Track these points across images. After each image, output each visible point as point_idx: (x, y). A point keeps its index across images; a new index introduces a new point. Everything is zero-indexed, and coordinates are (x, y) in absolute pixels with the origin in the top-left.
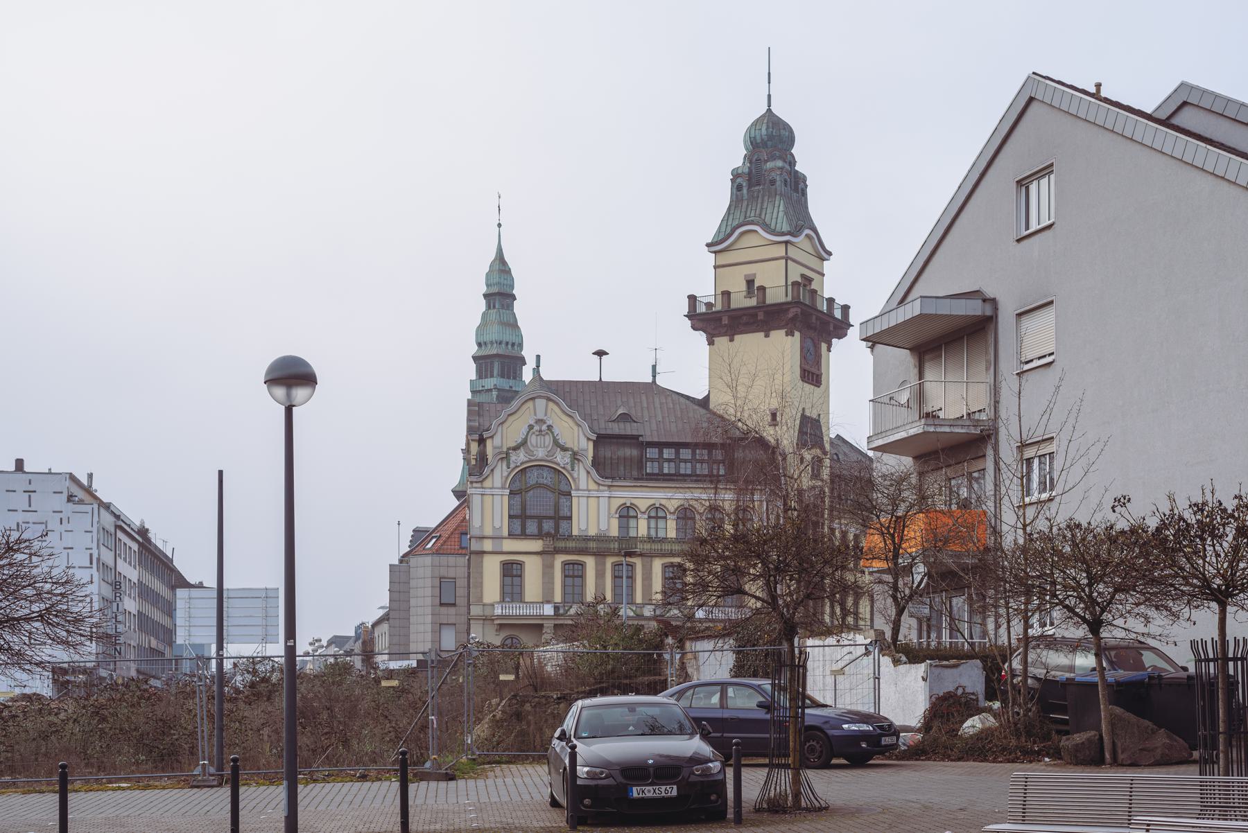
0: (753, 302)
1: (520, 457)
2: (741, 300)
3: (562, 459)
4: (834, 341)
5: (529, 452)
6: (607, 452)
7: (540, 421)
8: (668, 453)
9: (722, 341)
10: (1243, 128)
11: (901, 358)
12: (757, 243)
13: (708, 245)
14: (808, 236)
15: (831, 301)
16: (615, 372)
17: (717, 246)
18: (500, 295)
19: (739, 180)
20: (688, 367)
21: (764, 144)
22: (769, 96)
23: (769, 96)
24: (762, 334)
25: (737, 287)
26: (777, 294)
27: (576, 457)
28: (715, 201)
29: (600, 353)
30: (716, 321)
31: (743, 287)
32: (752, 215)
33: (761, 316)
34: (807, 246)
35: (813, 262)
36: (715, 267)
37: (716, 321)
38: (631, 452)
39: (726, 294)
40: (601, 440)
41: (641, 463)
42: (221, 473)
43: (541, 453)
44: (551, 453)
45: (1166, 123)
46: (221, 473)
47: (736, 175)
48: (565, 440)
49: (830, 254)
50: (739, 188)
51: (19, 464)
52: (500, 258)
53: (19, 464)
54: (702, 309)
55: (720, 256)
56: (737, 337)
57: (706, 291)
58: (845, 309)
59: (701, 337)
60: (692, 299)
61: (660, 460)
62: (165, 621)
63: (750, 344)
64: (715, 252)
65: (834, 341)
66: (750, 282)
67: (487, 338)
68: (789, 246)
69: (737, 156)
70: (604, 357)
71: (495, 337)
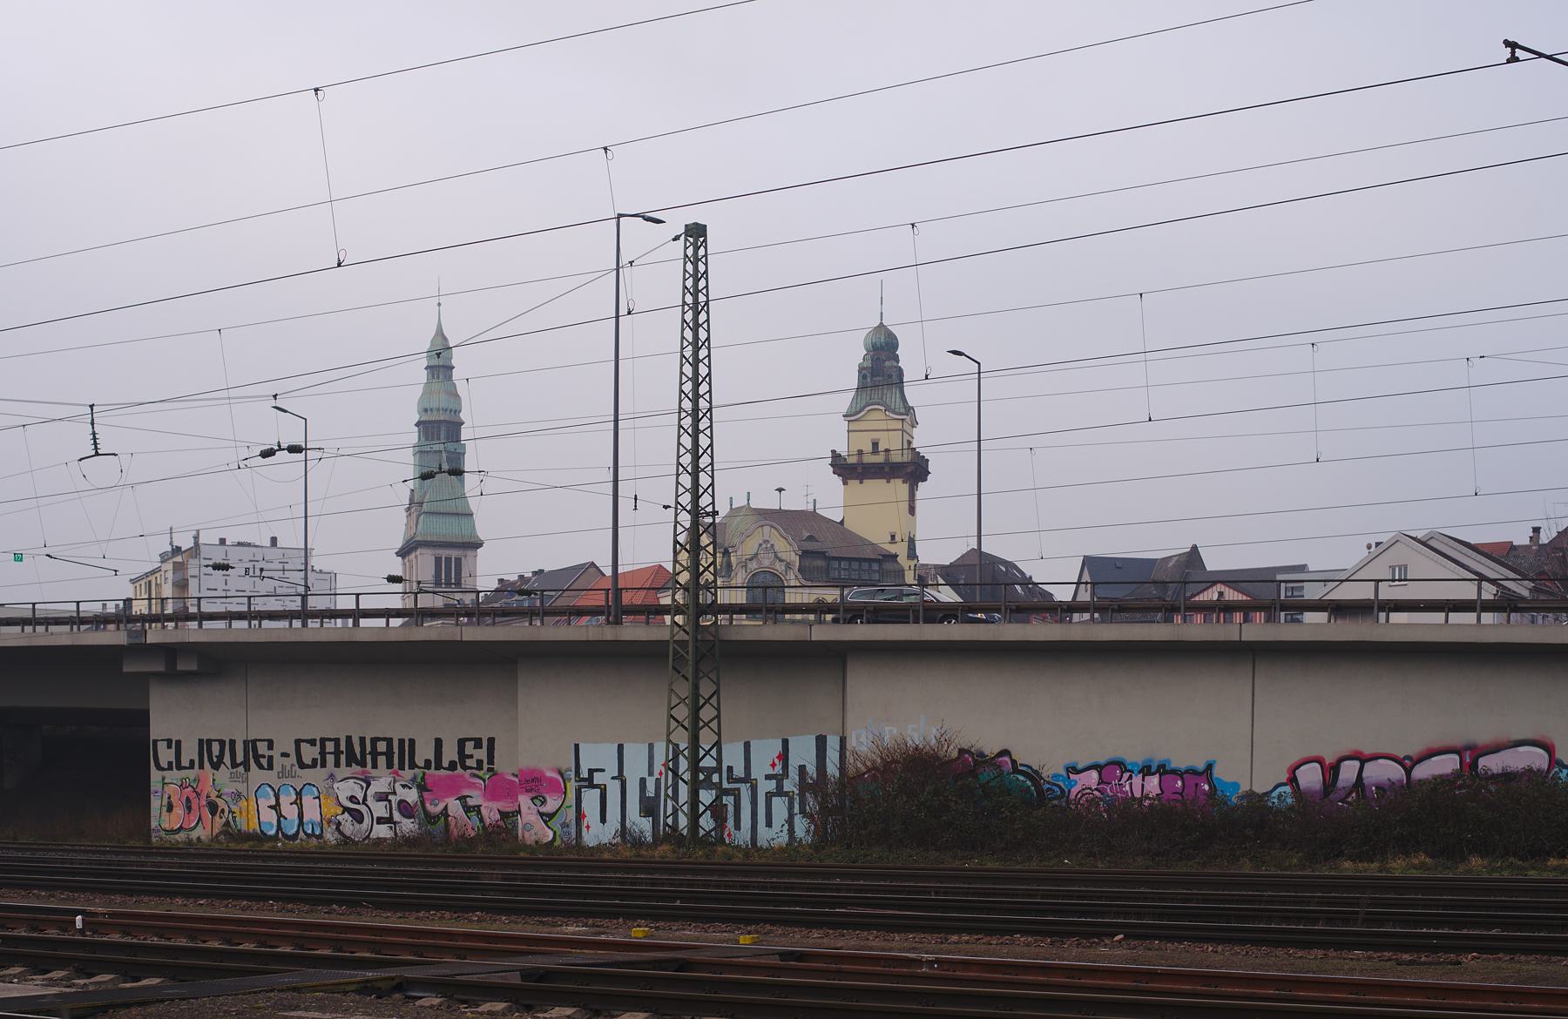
1: (753, 565)
3: (780, 567)
5: (759, 562)
6: (807, 563)
7: (766, 541)
8: (855, 565)
9: (854, 483)
12: (877, 419)
16: (788, 505)
18: (440, 365)
20: (830, 498)
21: (882, 348)
27: (788, 566)
29: (780, 490)
30: (846, 469)
37: (846, 469)
38: (820, 563)
39: (860, 452)
40: (805, 554)
41: (827, 571)
43: (766, 563)
44: (773, 563)
45: (1424, 544)
47: (861, 369)
48: (783, 556)
50: (864, 377)
51: (274, 541)
52: (440, 333)
53: (274, 541)
59: (838, 480)
61: (839, 569)
63: (876, 488)
66: (875, 445)
67: (435, 405)
71: (443, 405)
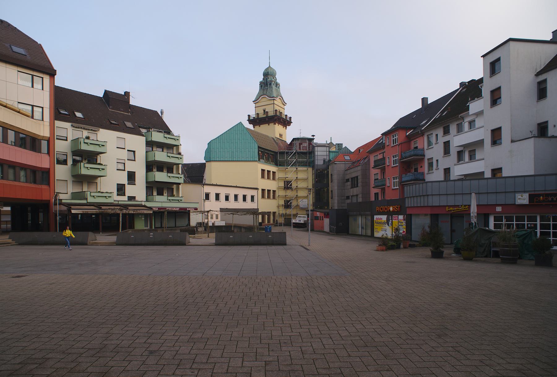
0: (265, 116)
2: (261, 116)
10: (5, 101)
11: (47, 139)
12: (264, 101)
15: (286, 116)
25: (261, 112)
26: (271, 114)
28: (256, 89)
31: (263, 112)
32: (265, 92)
33: (267, 119)
34: (279, 101)
35: (282, 106)
39: (258, 114)
54: (251, 118)
58: (290, 118)
60: (249, 116)
62: (74, 157)
66: (264, 111)
69: (261, 78)
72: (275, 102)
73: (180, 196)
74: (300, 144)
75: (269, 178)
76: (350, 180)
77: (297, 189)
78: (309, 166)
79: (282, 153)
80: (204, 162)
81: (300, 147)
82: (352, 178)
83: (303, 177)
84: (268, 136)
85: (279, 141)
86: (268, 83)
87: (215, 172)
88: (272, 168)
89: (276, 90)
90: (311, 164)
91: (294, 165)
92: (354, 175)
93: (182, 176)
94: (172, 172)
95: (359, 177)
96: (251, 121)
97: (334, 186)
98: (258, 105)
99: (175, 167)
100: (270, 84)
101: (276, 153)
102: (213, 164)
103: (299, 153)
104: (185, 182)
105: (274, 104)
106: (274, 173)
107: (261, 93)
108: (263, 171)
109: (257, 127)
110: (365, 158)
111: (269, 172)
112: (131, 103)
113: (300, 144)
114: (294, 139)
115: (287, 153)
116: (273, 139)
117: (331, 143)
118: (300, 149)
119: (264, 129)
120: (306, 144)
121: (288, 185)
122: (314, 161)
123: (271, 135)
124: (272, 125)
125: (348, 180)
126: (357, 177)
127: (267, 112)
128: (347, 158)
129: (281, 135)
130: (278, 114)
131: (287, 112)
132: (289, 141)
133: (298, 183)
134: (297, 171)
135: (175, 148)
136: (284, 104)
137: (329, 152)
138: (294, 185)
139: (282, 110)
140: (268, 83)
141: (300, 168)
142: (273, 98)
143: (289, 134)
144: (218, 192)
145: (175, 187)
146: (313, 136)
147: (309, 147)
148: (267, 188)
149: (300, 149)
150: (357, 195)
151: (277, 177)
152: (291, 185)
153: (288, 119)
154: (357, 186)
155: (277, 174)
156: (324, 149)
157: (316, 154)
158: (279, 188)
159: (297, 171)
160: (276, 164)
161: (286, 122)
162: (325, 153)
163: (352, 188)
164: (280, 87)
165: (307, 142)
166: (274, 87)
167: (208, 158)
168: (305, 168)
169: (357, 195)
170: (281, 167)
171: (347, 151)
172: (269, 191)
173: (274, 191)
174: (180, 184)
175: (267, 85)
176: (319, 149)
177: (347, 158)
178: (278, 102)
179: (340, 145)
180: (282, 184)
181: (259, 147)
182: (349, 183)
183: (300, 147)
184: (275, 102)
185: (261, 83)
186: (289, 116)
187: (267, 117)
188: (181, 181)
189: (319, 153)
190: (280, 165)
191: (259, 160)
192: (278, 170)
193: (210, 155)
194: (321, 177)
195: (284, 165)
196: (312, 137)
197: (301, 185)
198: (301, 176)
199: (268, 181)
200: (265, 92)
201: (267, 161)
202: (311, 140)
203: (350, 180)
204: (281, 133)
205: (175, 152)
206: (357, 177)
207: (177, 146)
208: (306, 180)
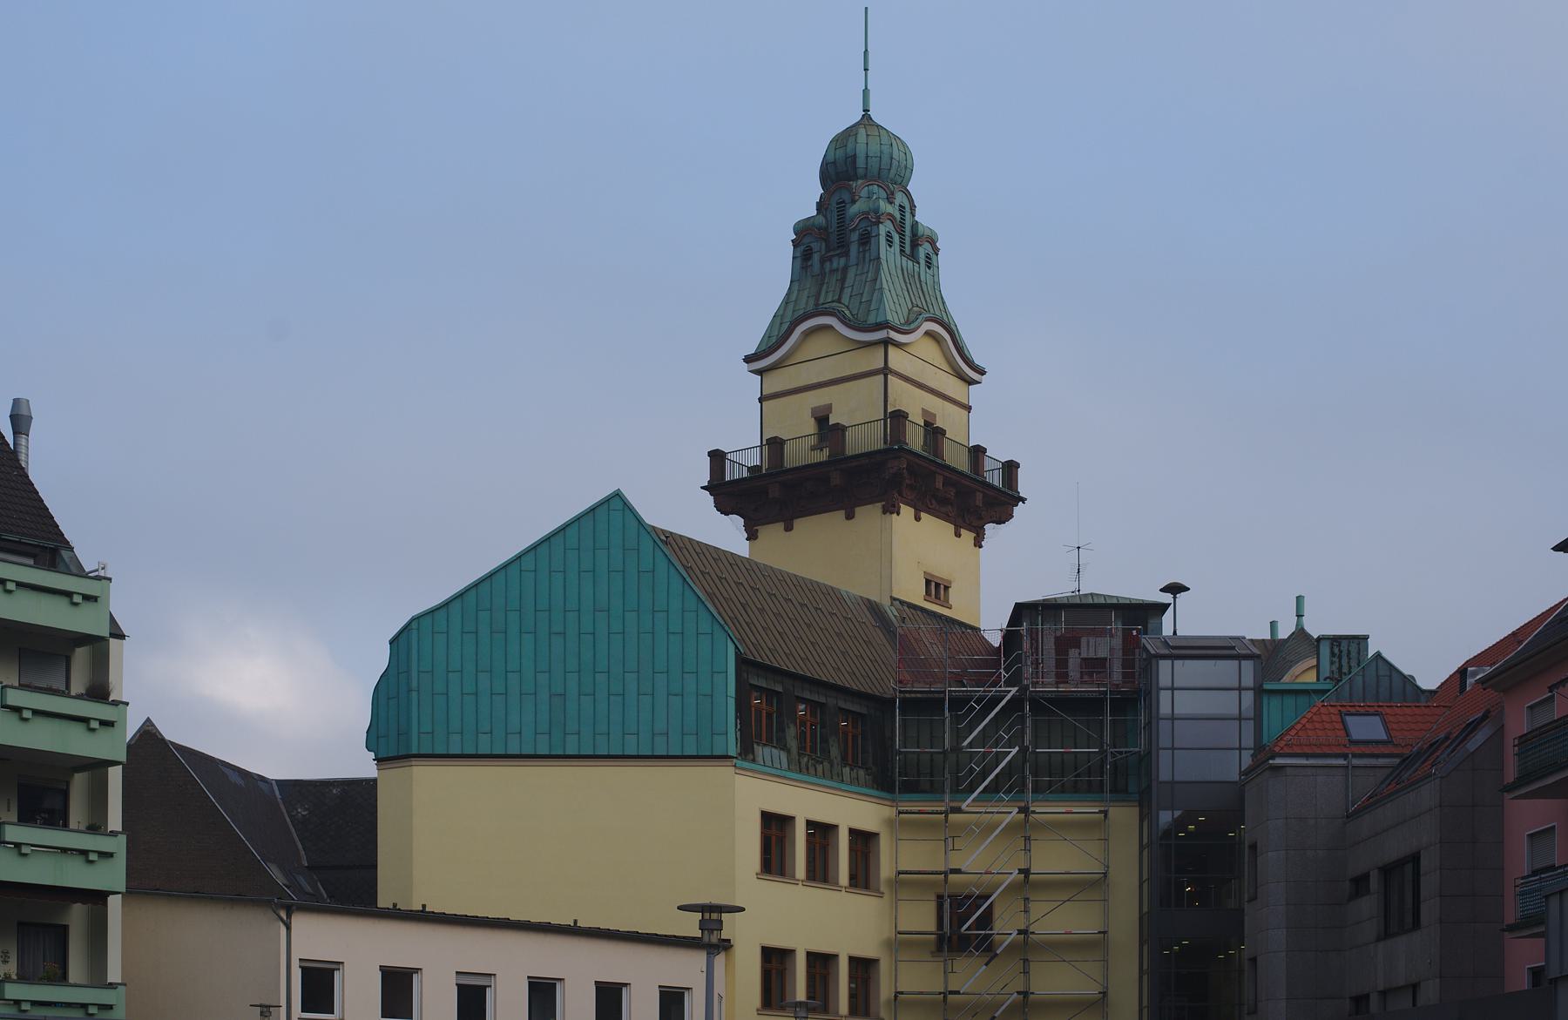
0: (823, 456)
2: (801, 453)
4: (990, 528)
12: (823, 356)
13: (748, 359)
14: (928, 334)
15: (978, 452)
17: (765, 358)
19: (806, 240)
22: (866, 92)
23: (866, 92)
24: (841, 514)
25: (796, 424)
26: (865, 438)
31: (810, 427)
32: (827, 297)
34: (930, 350)
35: (953, 386)
36: (760, 400)
42: (1299, 600)
46: (1299, 599)
49: (982, 372)
55: (768, 378)
56: (799, 524)
57: (743, 442)
58: (1010, 468)
60: (717, 457)
64: (760, 372)
65: (990, 528)
66: (822, 419)
68: (892, 350)
69: (805, 198)
70: (1181, 596)
72: (897, 359)
73: (114, 975)
74: (1064, 645)
75: (820, 872)
76: (1375, 882)
77: (1026, 948)
78: (1119, 791)
79: (923, 706)
80: (362, 766)
81: (1062, 663)
82: (1387, 871)
83: (1072, 872)
84: (831, 594)
85: (932, 624)
86: (856, 230)
87: (446, 829)
88: (851, 810)
89: (911, 280)
90: (1125, 778)
91: (1009, 784)
92: (1394, 848)
93: (119, 845)
94: (58, 819)
95: (1424, 863)
96: (728, 492)
97: (1269, 930)
98: (777, 382)
99: (79, 782)
100: (866, 239)
101: (885, 704)
102: (427, 778)
103: (1040, 705)
104: (141, 886)
105: (886, 371)
106: (863, 841)
107: (805, 304)
108: (775, 826)
109: (772, 534)
110: (1473, 727)
111: (821, 833)
112: (1430, 679)
113: (1064, 645)
114: (1021, 611)
115: (958, 703)
116: (874, 608)
117: (1300, 633)
118: (1062, 677)
119: (818, 551)
120: (1105, 645)
121: (962, 925)
122: (1146, 761)
123: (857, 584)
124: (869, 514)
125: (1360, 884)
126: (1415, 858)
127: (840, 429)
128: (1366, 728)
129: (937, 588)
130: (915, 440)
131: (991, 425)
132: (992, 623)
133: (1037, 909)
134: (1025, 832)
135: (81, 655)
136: (967, 371)
137: (1259, 691)
138: (1006, 926)
139: (947, 418)
140: (856, 230)
141: (1048, 810)
142: (877, 332)
143: (995, 577)
144: (399, 960)
145: (76, 916)
146: (1175, 589)
147: (1127, 664)
148: (801, 942)
149: (1062, 677)
150: (1415, 987)
151: (886, 869)
152: (986, 920)
153: (996, 479)
154: (1416, 924)
155: (884, 844)
156: (1224, 671)
157: (1165, 709)
158: (900, 943)
159: (1025, 832)
160: (885, 779)
161: (977, 497)
162: (1227, 704)
163: (1386, 934)
164: (943, 260)
165: (1116, 626)
166: (890, 256)
167: (393, 736)
168: (1086, 810)
169: (1415, 987)
170: (913, 804)
171: (1389, 686)
172: (821, 963)
173: (863, 968)
174: (97, 898)
175: (843, 246)
176: (1188, 671)
177: (1366, 728)
178: (917, 357)
179: (1347, 648)
180: (921, 917)
181: (743, 663)
182: (1368, 906)
183: (1062, 663)
184: (897, 359)
185: (805, 235)
186: (998, 452)
187: (840, 461)
188: (111, 876)
189: (1186, 704)
190: (910, 788)
191: (746, 751)
192: (890, 823)
193: (405, 719)
194: (1197, 865)
195: (934, 789)
196: (1167, 598)
197: (1057, 920)
198: (1054, 858)
199: (818, 896)
200: (827, 297)
201: (813, 759)
202: (1143, 614)
203: (1375, 882)
204: (941, 572)
205: (77, 687)
206: (1415, 858)
207: (98, 646)
208: (1094, 886)
